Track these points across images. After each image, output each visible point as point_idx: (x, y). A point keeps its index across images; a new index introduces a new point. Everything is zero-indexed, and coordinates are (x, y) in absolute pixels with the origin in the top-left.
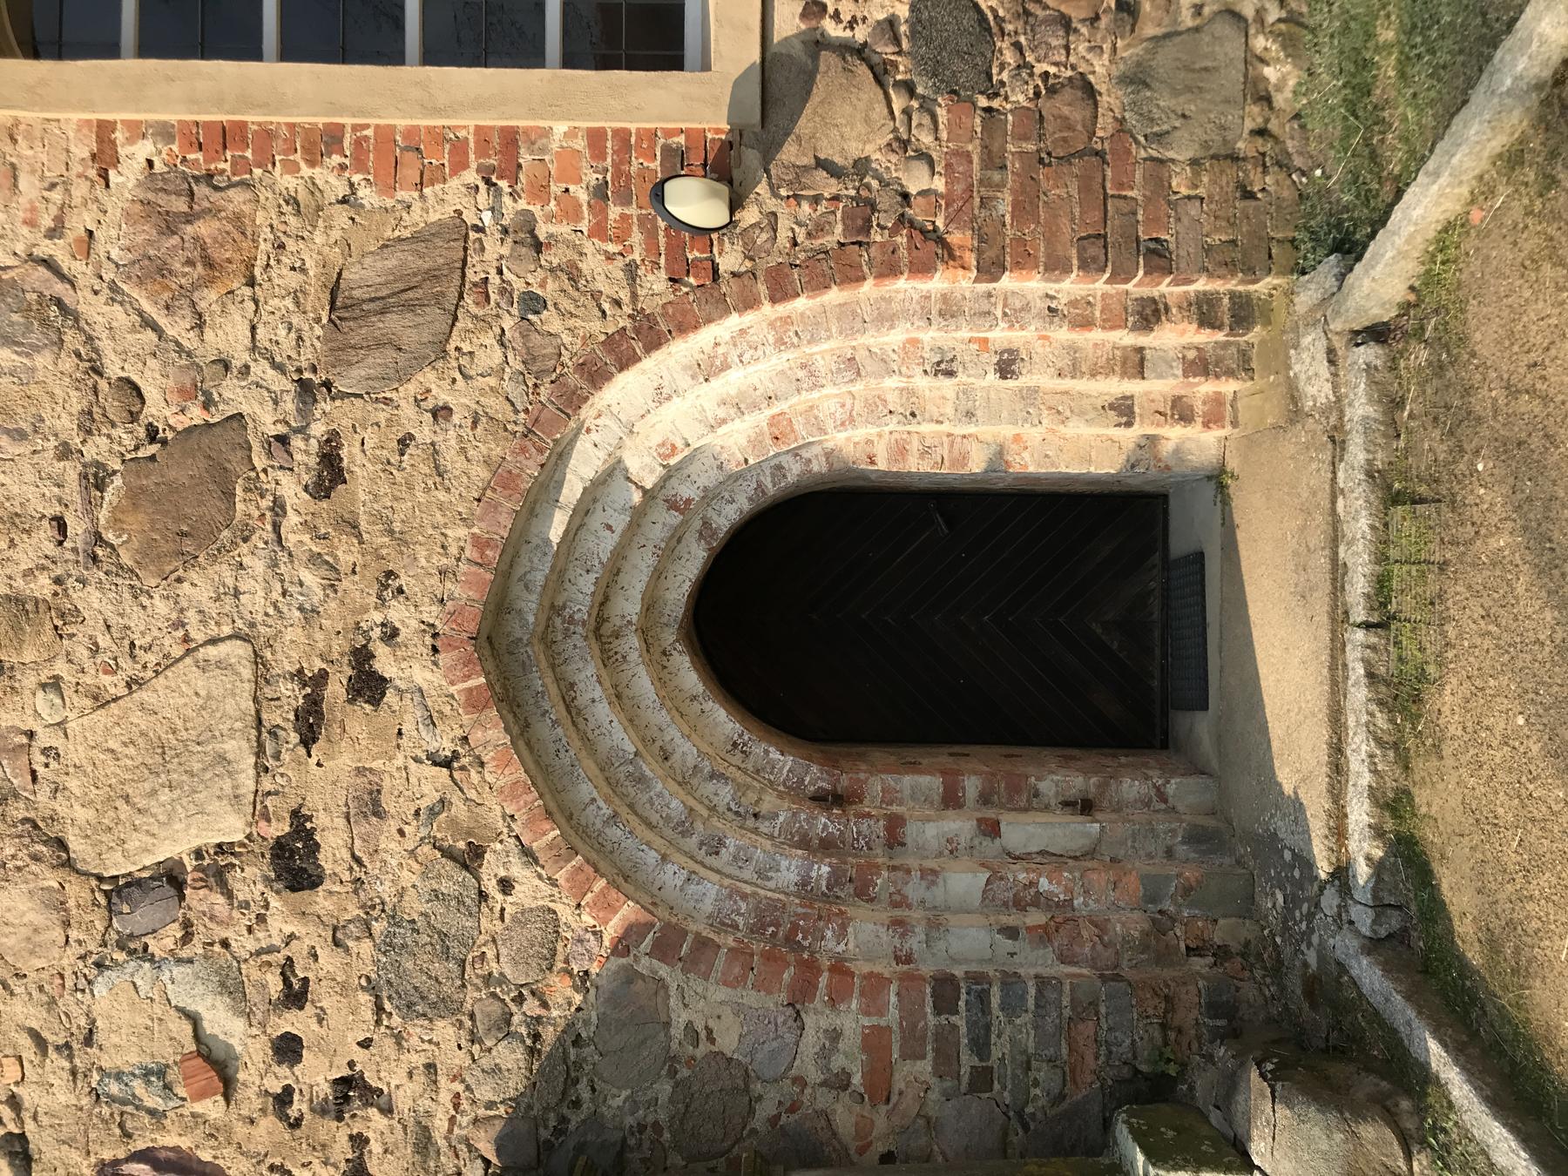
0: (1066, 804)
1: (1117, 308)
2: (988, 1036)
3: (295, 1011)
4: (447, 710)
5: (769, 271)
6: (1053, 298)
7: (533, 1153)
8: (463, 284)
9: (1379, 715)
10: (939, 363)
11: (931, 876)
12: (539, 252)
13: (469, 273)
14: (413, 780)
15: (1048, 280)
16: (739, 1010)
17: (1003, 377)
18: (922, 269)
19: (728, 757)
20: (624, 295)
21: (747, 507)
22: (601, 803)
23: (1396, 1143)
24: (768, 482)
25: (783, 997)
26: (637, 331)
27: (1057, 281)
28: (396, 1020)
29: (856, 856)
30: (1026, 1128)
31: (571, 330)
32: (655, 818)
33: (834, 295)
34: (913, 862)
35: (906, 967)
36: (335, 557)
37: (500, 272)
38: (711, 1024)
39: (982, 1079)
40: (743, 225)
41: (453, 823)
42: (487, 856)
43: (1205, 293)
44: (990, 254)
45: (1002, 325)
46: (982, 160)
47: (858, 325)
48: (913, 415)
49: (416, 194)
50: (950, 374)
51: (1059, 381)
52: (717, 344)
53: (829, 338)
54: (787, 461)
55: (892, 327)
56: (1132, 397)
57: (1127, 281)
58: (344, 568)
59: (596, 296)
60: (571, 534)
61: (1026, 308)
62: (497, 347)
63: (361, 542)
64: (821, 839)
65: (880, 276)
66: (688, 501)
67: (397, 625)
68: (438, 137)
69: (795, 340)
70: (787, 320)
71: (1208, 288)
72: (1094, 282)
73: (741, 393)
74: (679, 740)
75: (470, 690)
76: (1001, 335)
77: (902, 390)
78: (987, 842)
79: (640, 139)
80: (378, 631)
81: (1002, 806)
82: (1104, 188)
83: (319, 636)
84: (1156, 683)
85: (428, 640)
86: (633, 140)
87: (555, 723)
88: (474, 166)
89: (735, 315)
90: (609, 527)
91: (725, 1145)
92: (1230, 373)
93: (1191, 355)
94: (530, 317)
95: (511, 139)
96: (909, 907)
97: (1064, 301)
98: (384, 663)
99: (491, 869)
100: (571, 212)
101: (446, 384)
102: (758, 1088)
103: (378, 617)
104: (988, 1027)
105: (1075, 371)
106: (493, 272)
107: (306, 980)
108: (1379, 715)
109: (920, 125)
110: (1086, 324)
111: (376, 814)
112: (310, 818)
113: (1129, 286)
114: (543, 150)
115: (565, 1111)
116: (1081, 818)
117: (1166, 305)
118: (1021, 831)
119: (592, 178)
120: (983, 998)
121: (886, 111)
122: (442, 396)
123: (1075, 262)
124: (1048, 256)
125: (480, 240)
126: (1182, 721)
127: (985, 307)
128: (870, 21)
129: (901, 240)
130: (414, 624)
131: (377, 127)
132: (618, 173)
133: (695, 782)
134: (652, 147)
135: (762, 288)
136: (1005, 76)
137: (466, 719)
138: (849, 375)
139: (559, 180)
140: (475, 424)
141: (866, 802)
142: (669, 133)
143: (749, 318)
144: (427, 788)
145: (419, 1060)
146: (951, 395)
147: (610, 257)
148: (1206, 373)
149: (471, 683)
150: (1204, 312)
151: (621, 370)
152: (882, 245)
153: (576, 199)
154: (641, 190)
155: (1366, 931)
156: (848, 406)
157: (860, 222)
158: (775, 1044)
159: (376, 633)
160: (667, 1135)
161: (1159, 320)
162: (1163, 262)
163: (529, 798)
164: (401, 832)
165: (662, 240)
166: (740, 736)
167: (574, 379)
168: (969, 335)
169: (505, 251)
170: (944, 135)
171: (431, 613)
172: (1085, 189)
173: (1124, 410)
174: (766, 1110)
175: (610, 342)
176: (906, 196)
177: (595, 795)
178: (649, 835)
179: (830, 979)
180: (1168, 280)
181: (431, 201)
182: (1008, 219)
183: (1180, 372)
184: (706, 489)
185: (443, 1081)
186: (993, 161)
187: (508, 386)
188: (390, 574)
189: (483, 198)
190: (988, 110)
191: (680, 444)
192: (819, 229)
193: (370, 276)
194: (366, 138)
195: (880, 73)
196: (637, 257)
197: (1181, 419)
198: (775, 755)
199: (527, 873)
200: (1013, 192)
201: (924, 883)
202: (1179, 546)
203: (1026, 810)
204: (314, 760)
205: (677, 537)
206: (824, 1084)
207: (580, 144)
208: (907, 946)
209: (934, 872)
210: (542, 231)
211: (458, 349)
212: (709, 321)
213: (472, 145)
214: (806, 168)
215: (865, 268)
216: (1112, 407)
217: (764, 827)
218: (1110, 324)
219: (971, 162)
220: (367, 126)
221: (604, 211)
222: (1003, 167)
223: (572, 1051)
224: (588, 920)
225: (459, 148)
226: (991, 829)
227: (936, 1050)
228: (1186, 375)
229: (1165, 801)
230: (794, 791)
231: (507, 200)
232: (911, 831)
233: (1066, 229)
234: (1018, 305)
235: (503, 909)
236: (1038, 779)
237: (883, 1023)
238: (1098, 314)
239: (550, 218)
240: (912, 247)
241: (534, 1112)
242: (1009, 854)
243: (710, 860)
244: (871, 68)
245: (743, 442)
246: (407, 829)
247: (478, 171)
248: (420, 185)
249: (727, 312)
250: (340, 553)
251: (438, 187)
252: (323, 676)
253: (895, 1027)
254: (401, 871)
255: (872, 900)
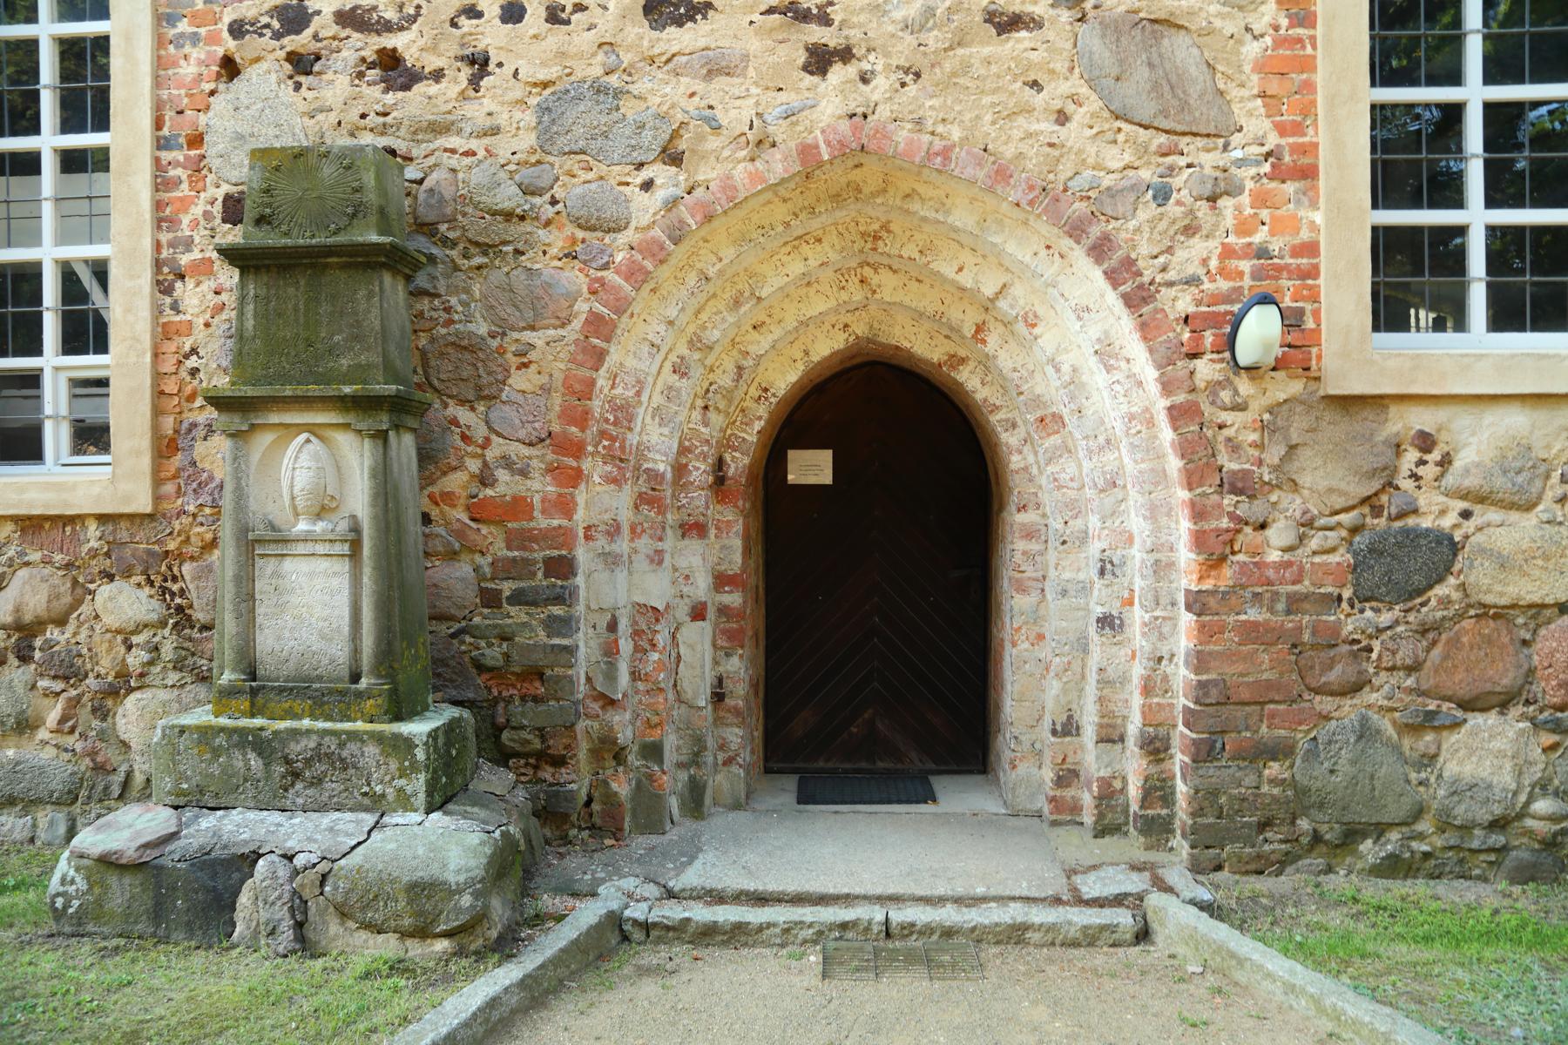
0: (720, 680)
1: (1160, 717)
2: (527, 603)
3: (544, 14)
4: (799, 128)
5: (1196, 404)
6: (1171, 660)
7: (428, 220)
8: (1176, 133)
9: (811, 931)
10: (1111, 562)
11: (657, 558)
12: (1208, 200)
13: (1187, 139)
14: (738, 103)
15: (1187, 655)
16: (546, 390)
17: (1098, 620)
18: (1200, 540)
19: (755, 384)
20: (1172, 275)
21: (979, 397)
22: (718, 266)
23: (456, 924)
24: (1001, 415)
25: (556, 428)
26: (1141, 287)
27: (1187, 663)
28: (533, 101)
29: (673, 495)
30: (453, 636)
31: (1139, 230)
32: (704, 316)
33: (1174, 464)
34: (667, 545)
35: (581, 533)
36: (931, 29)
37: (1189, 166)
38: (533, 367)
39: (491, 599)
40: (1236, 380)
41: (701, 138)
42: (674, 169)
43: (1173, 793)
44: (1212, 602)
45: (1147, 616)
46: (1296, 593)
47: (1147, 487)
48: (1064, 542)
49: (1255, 91)
50: (1102, 572)
51: (1094, 669)
52: (1128, 361)
53: (1136, 462)
54: (1021, 432)
55: (1145, 518)
56: (1078, 735)
57: (1187, 724)
58: (923, 37)
59: (1169, 250)
60: (954, 236)
61: (1162, 637)
62: (1121, 164)
63: (945, 50)
64: (686, 465)
65: (1193, 504)
66: (984, 342)
67: (873, 83)
68: (1308, 110)
69: (1133, 431)
70: (1151, 423)
71: (1179, 796)
72: (1185, 696)
73: (1083, 385)
74: (770, 338)
75: (817, 147)
76: (1137, 616)
77: (1086, 533)
78: (687, 609)
79: (1311, 288)
80: (869, 67)
81: (716, 625)
82: (1271, 702)
83: (862, 18)
84: (821, 764)
85: (860, 110)
86: (1310, 282)
87: (787, 225)
88: (1283, 142)
89: (1156, 374)
90: (961, 269)
91: (436, 382)
92: (1100, 816)
93: (1117, 784)
94: (1150, 192)
95: (1308, 173)
96: (632, 540)
97: (1168, 670)
98: (838, 74)
99: (661, 173)
100: (1244, 228)
101: (1087, 121)
102: (481, 408)
103: (879, 68)
104: (534, 604)
105: (1104, 683)
106: (1189, 160)
107: (568, 22)
108: (811, 931)
109: (1326, 538)
110: (1147, 690)
111: (710, 71)
112: (705, 17)
113: (1181, 727)
114: (1298, 202)
115: (461, 246)
116: (709, 691)
117: (1163, 760)
118: (697, 640)
119: (1275, 246)
120: (559, 600)
121: (1338, 507)
122: (1079, 115)
123: (1204, 677)
124: (1210, 653)
125: (1216, 148)
126: (791, 782)
127: (1164, 601)
128: (1417, 493)
129: (1225, 523)
130: (875, 97)
131: (1314, 57)
132: (1279, 269)
133: (735, 353)
134: (1303, 299)
135: (1181, 398)
136: (1369, 614)
137: (792, 144)
138: (1101, 483)
139: (1272, 217)
140: (1051, 145)
141: (719, 507)
142: (1316, 314)
143: (1153, 388)
144: (733, 113)
145: (502, 119)
146: (1082, 576)
147: (1205, 262)
148: (1100, 798)
149: (823, 146)
150: (1158, 790)
151: (1105, 273)
152: (1220, 506)
153: (1255, 231)
154: (1266, 286)
155: (627, 913)
156: (1071, 484)
157: (1240, 485)
158: (517, 422)
159: (866, 66)
160: (443, 331)
161: (1150, 753)
162: (1203, 754)
163: (723, 202)
164: (692, 95)
165: (1222, 308)
166: (774, 395)
167: (1095, 231)
168: (1137, 589)
169: (1208, 171)
170: (1317, 559)
171: (884, 112)
172: (1269, 685)
173: (1068, 728)
174: (464, 415)
175: (1129, 263)
176: (1263, 526)
177: (725, 261)
178: (690, 311)
179: (572, 468)
180: (1187, 759)
181: (1250, 105)
182: (1243, 617)
183: (1102, 774)
184: (995, 357)
185: (487, 141)
186: (1295, 603)
187: (1088, 173)
188: (918, 75)
189: (1256, 150)
190: (1340, 599)
191: (1036, 331)
192: (1234, 447)
193: (1180, 55)
194: (1304, 47)
195: (1370, 502)
196: (1207, 286)
197: (1059, 777)
198: (758, 425)
199: (659, 204)
200: (1267, 621)
201: (651, 553)
202: (940, 784)
203: (714, 645)
204: (756, 17)
205: (952, 332)
206: (485, 464)
207: (1305, 235)
208: (599, 536)
209: (660, 562)
210: (1226, 203)
211: (1119, 130)
212: (1151, 351)
213: (1301, 140)
214: (1286, 438)
215: (1199, 491)
216: (1070, 717)
217: (696, 415)
218: (1147, 711)
219: (1294, 583)
220: (1314, 47)
221: (1246, 256)
222: (1288, 612)
223: (510, 248)
224: (619, 258)
225: (1298, 129)
226: (698, 613)
227: (514, 559)
228: (1100, 779)
229: (724, 764)
230: (726, 443)
231: (1253, 171)
232: (694, 545)
233: (1231, 670)
234: (1165, 630)
235: (628, 184)
236: (741, 656)
237: (536, 513)
238: (1156, 700)
239: (1238, 209)
240: (1219, 532)
241: (460, 217)
242: (677, 629)
243: (668, 367)
244: (1376, 494)
245: (1038, 390)
246: (696, 99)
247: (1278, 146)
248: (1263, 95)
249: (1159, 367)
250: (935, 32)
251: (1263, 110)
252: (825, 20)
253: (532, 524)
254: (664, 94)
255: (636, 507)
